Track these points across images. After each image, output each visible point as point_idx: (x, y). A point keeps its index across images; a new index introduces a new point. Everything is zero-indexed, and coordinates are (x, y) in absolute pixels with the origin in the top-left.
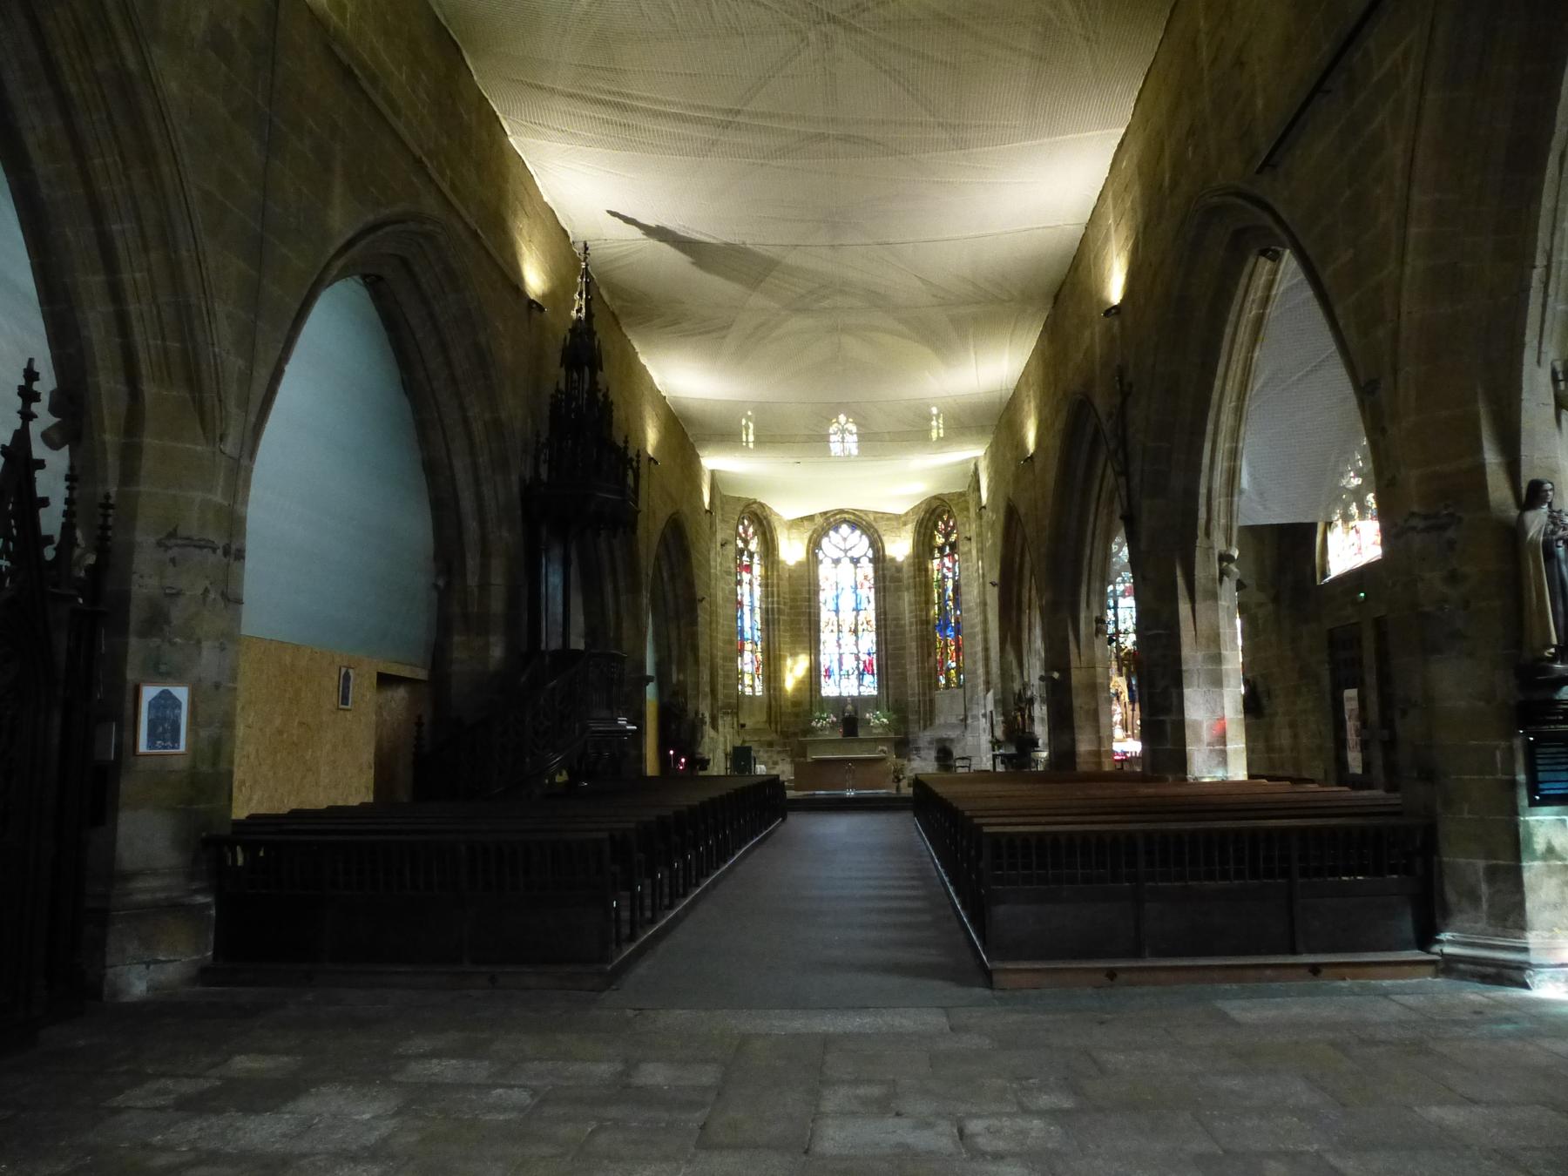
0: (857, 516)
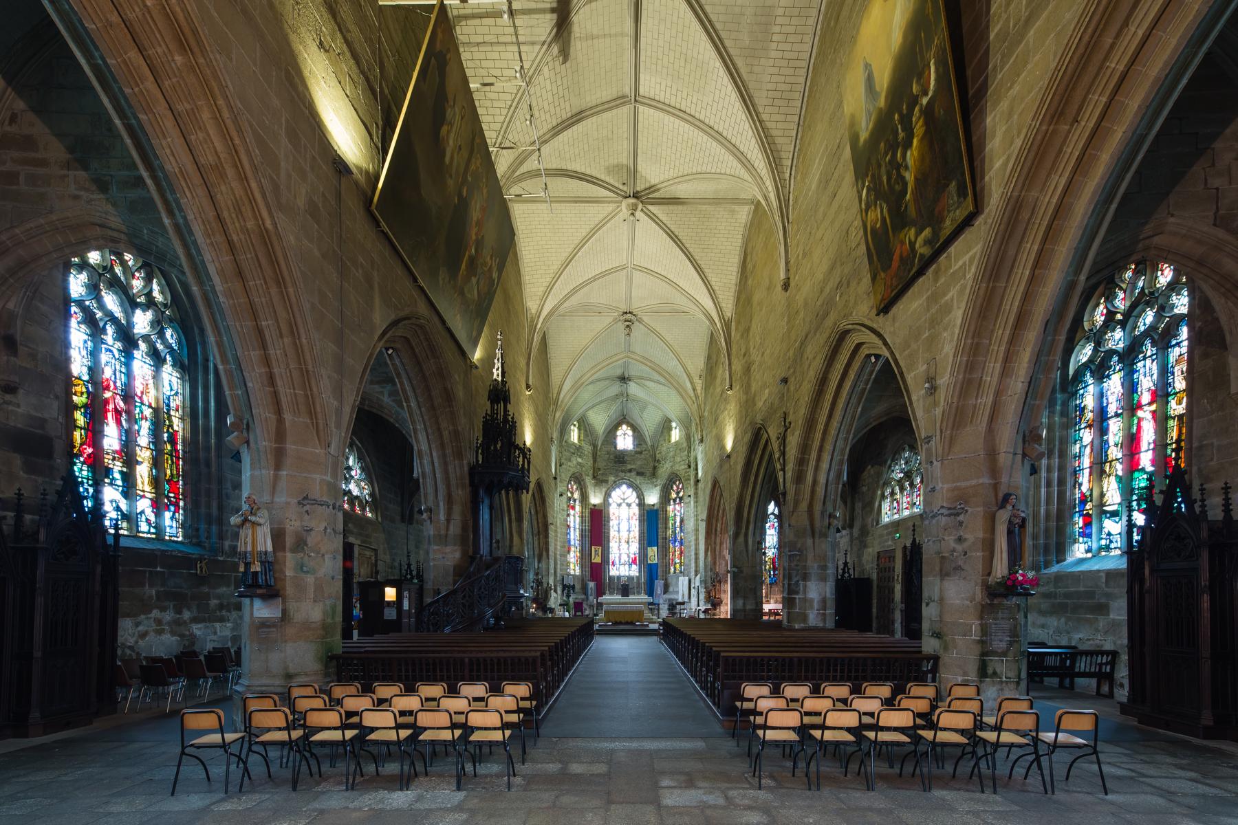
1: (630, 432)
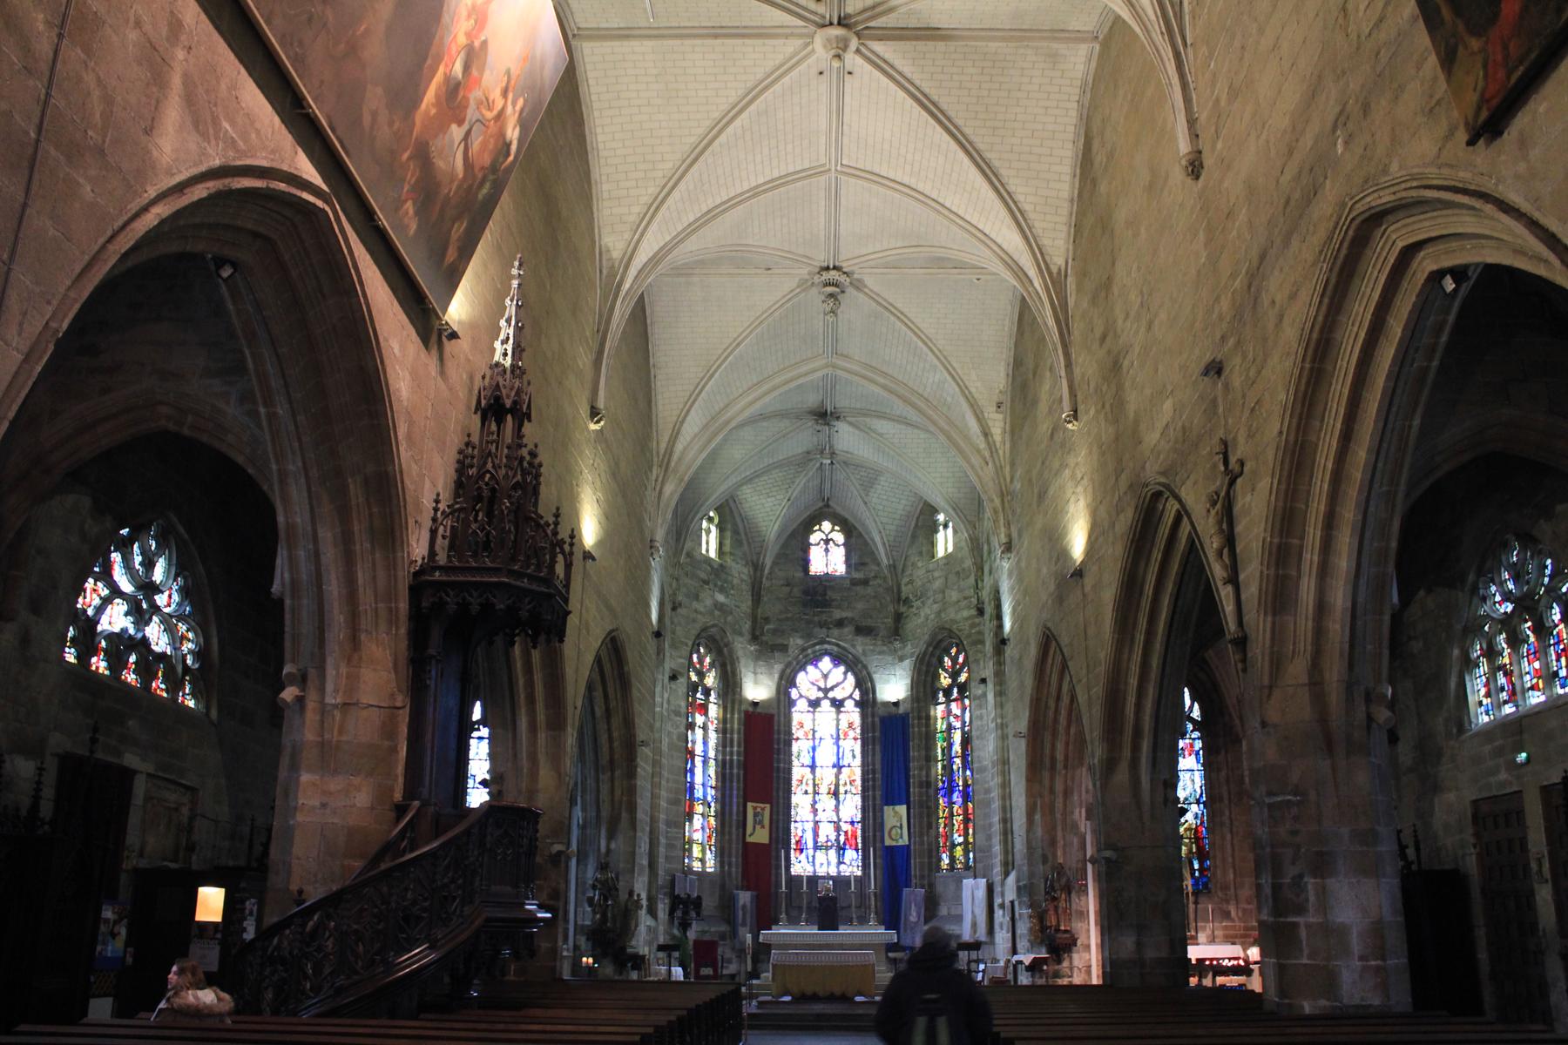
0: (844, 648)
1: (839, 537)
